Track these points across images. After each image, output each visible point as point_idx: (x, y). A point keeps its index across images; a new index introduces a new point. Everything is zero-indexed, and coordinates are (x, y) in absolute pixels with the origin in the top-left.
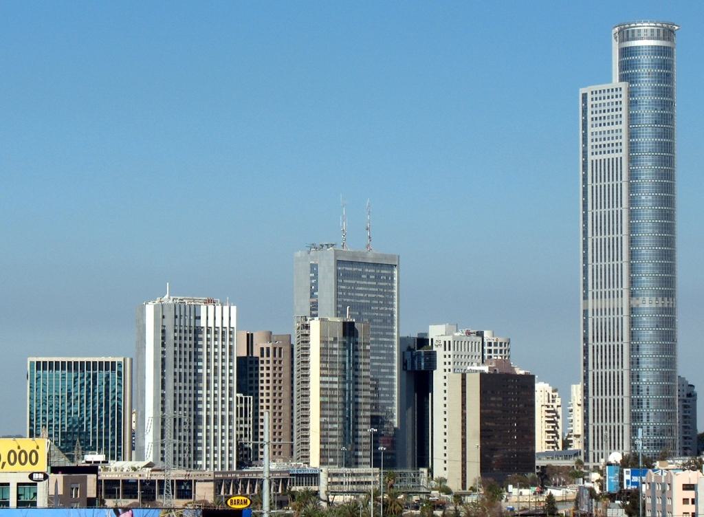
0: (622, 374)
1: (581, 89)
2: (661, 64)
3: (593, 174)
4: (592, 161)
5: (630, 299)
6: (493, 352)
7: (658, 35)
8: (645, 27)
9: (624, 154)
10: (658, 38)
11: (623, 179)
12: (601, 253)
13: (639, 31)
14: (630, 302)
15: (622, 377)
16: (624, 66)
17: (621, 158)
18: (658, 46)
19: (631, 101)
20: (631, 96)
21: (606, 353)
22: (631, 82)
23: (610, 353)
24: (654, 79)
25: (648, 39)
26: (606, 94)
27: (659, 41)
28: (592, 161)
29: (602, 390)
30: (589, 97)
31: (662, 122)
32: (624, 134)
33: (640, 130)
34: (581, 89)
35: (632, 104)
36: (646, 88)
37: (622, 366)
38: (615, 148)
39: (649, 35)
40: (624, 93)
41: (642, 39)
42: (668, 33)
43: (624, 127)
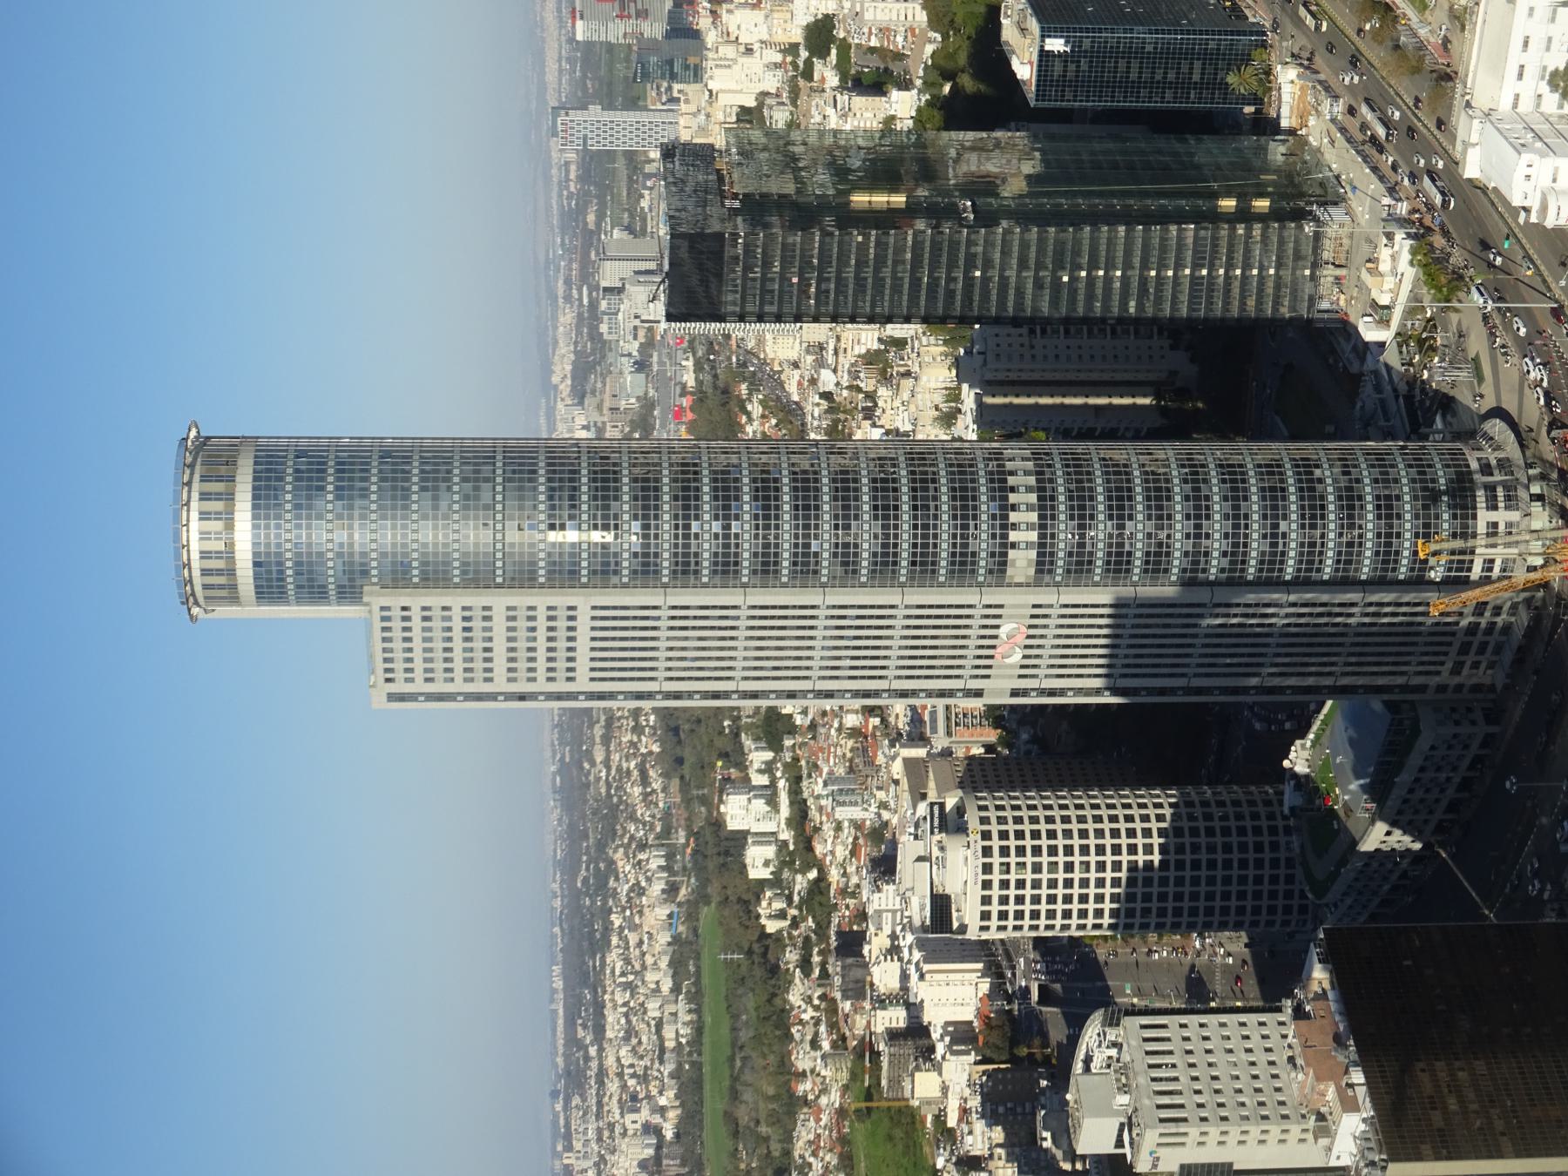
0: (834, 607)
1: (375, 706)
2: (394, 488)
3: (709, 678)
4: (592, 679)
5: (1009, 585)
6: (1204, 864)
7: (218, 497)
8: (196, 534)
9: (584, 602)
10: (229, 497)
11: (895, 600)
12: (613, 659)
13: (205, 555)
14: (1019, 585)
15: (762, 607)
16: (313, 591)
17: (594, 608)
18: (255, 497)
19: (422, 579)
20: (535, 579)
21: (1078, 636)
22: (365, 573)
23: (869, 627)
24: (356, 513)
25: (230, 526)
26: (398, 645)
27: (238, 496)
28: (592, 679)
29: (859, 648)
30: (399, 687)
31: (403, 489)
32: (521, 599)
33: (512, 554)
34: (375, 706)
35: (435, 575)
36: (278, 536)
37: (655, 608)
38: (562, 624)
39: (217, 526)
40: (396, 600)
41: (230, 545)
42: (211, 460)
43: (500, 601)
